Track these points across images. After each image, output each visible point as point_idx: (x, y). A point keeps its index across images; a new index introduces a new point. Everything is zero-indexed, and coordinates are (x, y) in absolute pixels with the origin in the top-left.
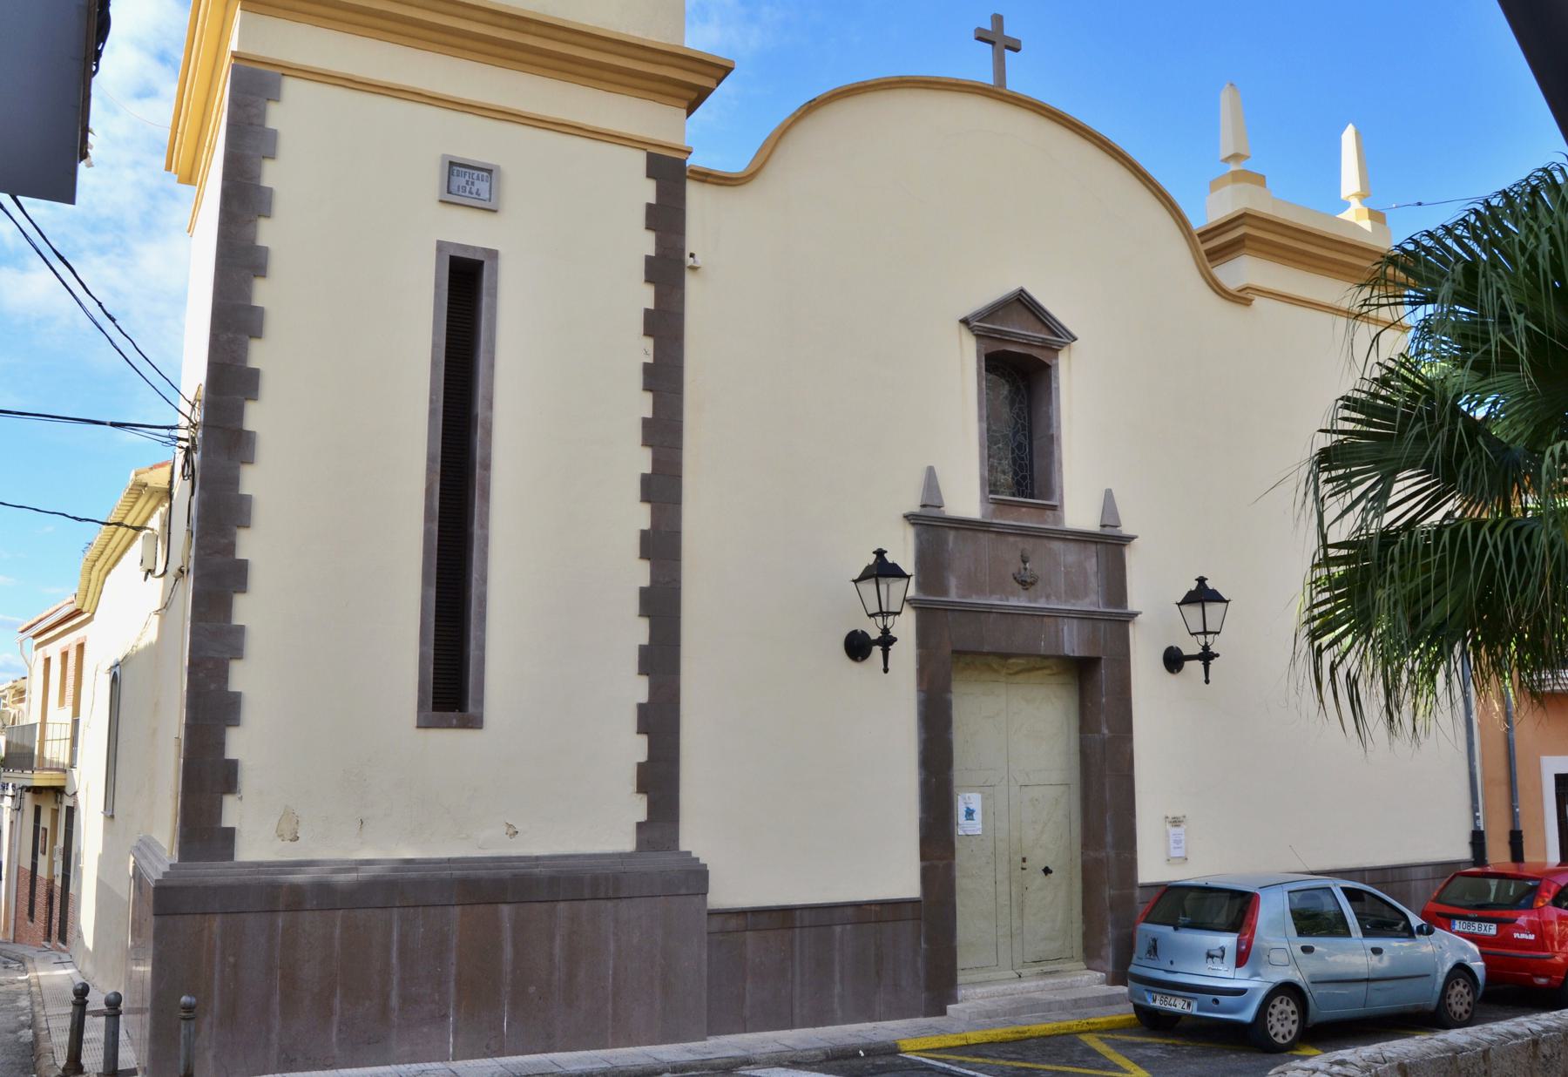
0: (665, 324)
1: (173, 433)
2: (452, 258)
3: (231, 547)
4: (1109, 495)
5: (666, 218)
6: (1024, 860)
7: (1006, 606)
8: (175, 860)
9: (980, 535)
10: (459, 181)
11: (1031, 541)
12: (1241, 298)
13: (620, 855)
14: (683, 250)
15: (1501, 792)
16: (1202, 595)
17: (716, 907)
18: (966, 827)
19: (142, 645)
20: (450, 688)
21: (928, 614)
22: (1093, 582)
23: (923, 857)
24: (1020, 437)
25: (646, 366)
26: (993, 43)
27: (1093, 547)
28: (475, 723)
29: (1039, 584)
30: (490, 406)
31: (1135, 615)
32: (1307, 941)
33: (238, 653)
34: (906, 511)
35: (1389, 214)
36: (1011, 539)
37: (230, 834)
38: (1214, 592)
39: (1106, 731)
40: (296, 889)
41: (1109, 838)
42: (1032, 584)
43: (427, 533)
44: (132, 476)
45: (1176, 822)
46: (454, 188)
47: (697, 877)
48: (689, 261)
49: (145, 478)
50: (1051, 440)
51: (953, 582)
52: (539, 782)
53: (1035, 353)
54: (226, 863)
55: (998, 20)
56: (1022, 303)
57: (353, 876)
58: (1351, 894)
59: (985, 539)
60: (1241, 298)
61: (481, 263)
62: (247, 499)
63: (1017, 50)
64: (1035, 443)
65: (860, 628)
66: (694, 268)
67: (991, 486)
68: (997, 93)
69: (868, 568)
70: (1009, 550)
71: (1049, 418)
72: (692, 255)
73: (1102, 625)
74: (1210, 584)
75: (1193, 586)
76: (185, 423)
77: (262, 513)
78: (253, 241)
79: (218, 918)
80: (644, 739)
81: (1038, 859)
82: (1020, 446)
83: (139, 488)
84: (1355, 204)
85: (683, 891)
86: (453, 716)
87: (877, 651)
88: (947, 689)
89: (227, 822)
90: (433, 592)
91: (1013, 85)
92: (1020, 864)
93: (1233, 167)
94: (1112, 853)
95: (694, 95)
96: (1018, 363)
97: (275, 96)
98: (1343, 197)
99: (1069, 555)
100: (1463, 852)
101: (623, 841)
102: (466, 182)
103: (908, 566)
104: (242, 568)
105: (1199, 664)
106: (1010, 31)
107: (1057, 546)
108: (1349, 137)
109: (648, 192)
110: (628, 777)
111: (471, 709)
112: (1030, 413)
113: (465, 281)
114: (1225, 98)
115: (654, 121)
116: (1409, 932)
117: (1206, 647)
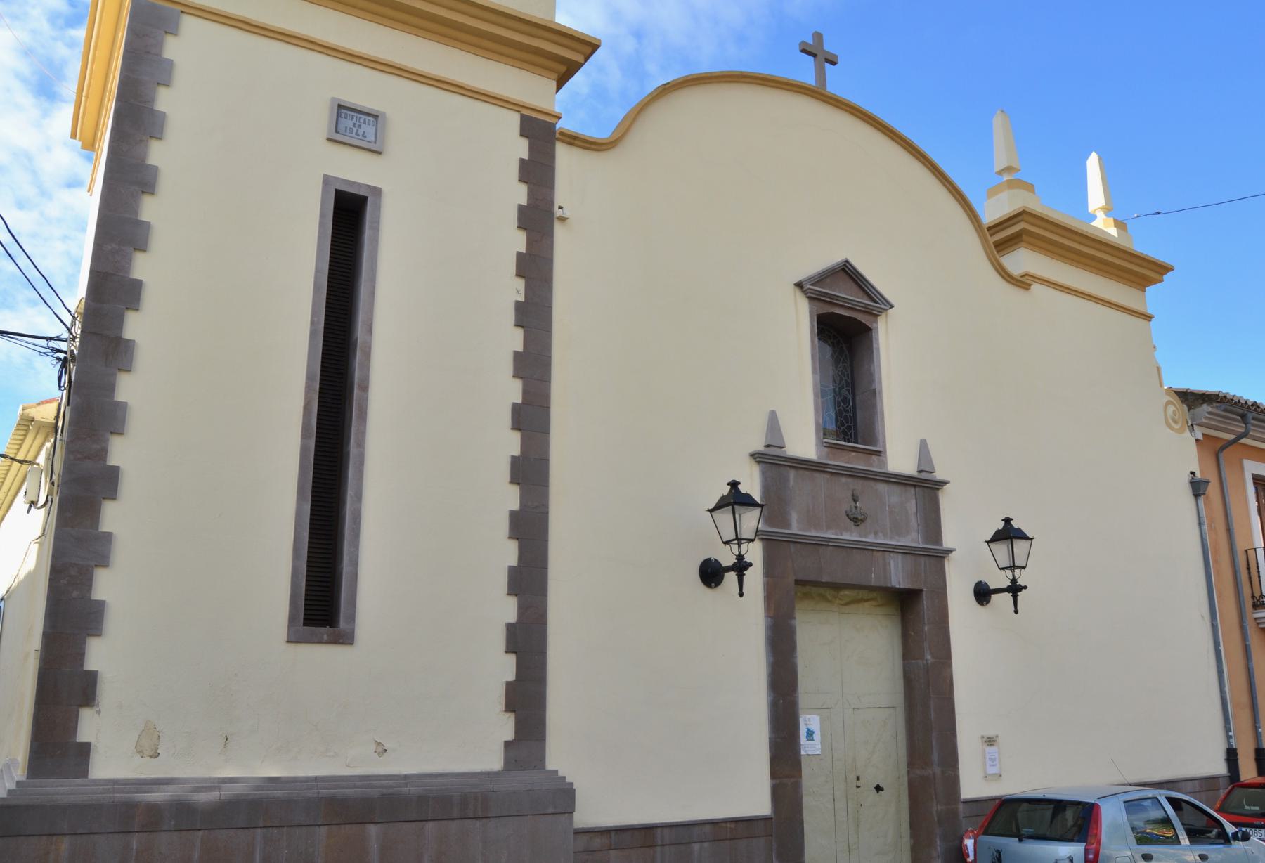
0: (535, 267)
1: (53, 344)
2: (337, 192)
3: (103, 453)
4: (923, 445)
5: (538, 173)
6: (858, 778)
7: (840, 542)
8: (24, 779)
9: (817, 475)
10: (347, 123)
11: (860, 482)
12: (1022, 282)
13: (489, 775)
14: (552, 203)
15: (1246, 715)
16: (1008, 533)
17: (581, 826)
18: (809, 747)
19: (21, 576)
20: (322, 603)
21: (772, 543)
22: (913, 522)
23: (774, 775)
24: (844, 392)
25: (518, 304)
26: (814, 55)
27: (912, 490)
28: (346, 639)
29: (868, 521)
30: (370, 331)
31: (949, 551)
32: (1146, 849)
33: (104, 562)
34: (752, 450)
35: (1130, 225)
36: (844, 480)
37: (85, 749)
38: (1019, 530)
39: (929, 657)
40: (154, 810)
41: (935, 757)
42: (862, 521)
43: (304, 449)
44: (20, 410)
45: (990, 741)
46: (341, 128)
47: (564, 796)
48: (558, 213)
49: (32, 412)
50: (874, 394)
51: (794, 518)
52: (405, 704)
53: (860, 317)
54: (79, 781)
55: (818, 37)
56: (846, 271)
57: (215, 795)
58: (1175, 803)
59: (821, 478)
60: (1022, 282)
61: (365, 199)
62: (123, 407)
63: (834, 63)
64: (858, 398)
65: (713, 556)
66: (562, 219)
67: (823, 432)
68: (818, 94)
69: (723, 498)
70: (843, 488)
71: (871, 375)
72: (560, 208)
73: (922, 560)
74: (1015, 524)
75: (1001, 525)
76: (66, 335)
77: (136, 421)
78: (144, 160)
79: (66, 840)
80: (512, 659)
81: (869, 781)
82: (845, 400)
83: (27, 423)
84: (1101, 215)
85: (550, 810)
86: (325, 631)
87: (731, 577)
88: (791, 616)
89: (83, 735)
90: (307, 507)
91: (833, 88)
92: (855, 783)
93: (1006, 177)
94: (938, 770)
95: (563, 69)
96: (844, 327)
97: (173, 30)
98: (1090, 209)
99: (893, 495)
100: (1221, 769)
101: (493, 761)
102: (352, 124)
103: (757, 497)
104: (112, 476)
105: (1008, 597)
106: (829, 46)
107: (882, 487)
108: (1093, 163)
109: (522, 149)
110: (497, 696)
111: (342, 624)
112: (852, 371)
113: (349, 215)
114: (998, 121)
115: (532, 88)
116: (1224, 838)
117: (1014, 581)
